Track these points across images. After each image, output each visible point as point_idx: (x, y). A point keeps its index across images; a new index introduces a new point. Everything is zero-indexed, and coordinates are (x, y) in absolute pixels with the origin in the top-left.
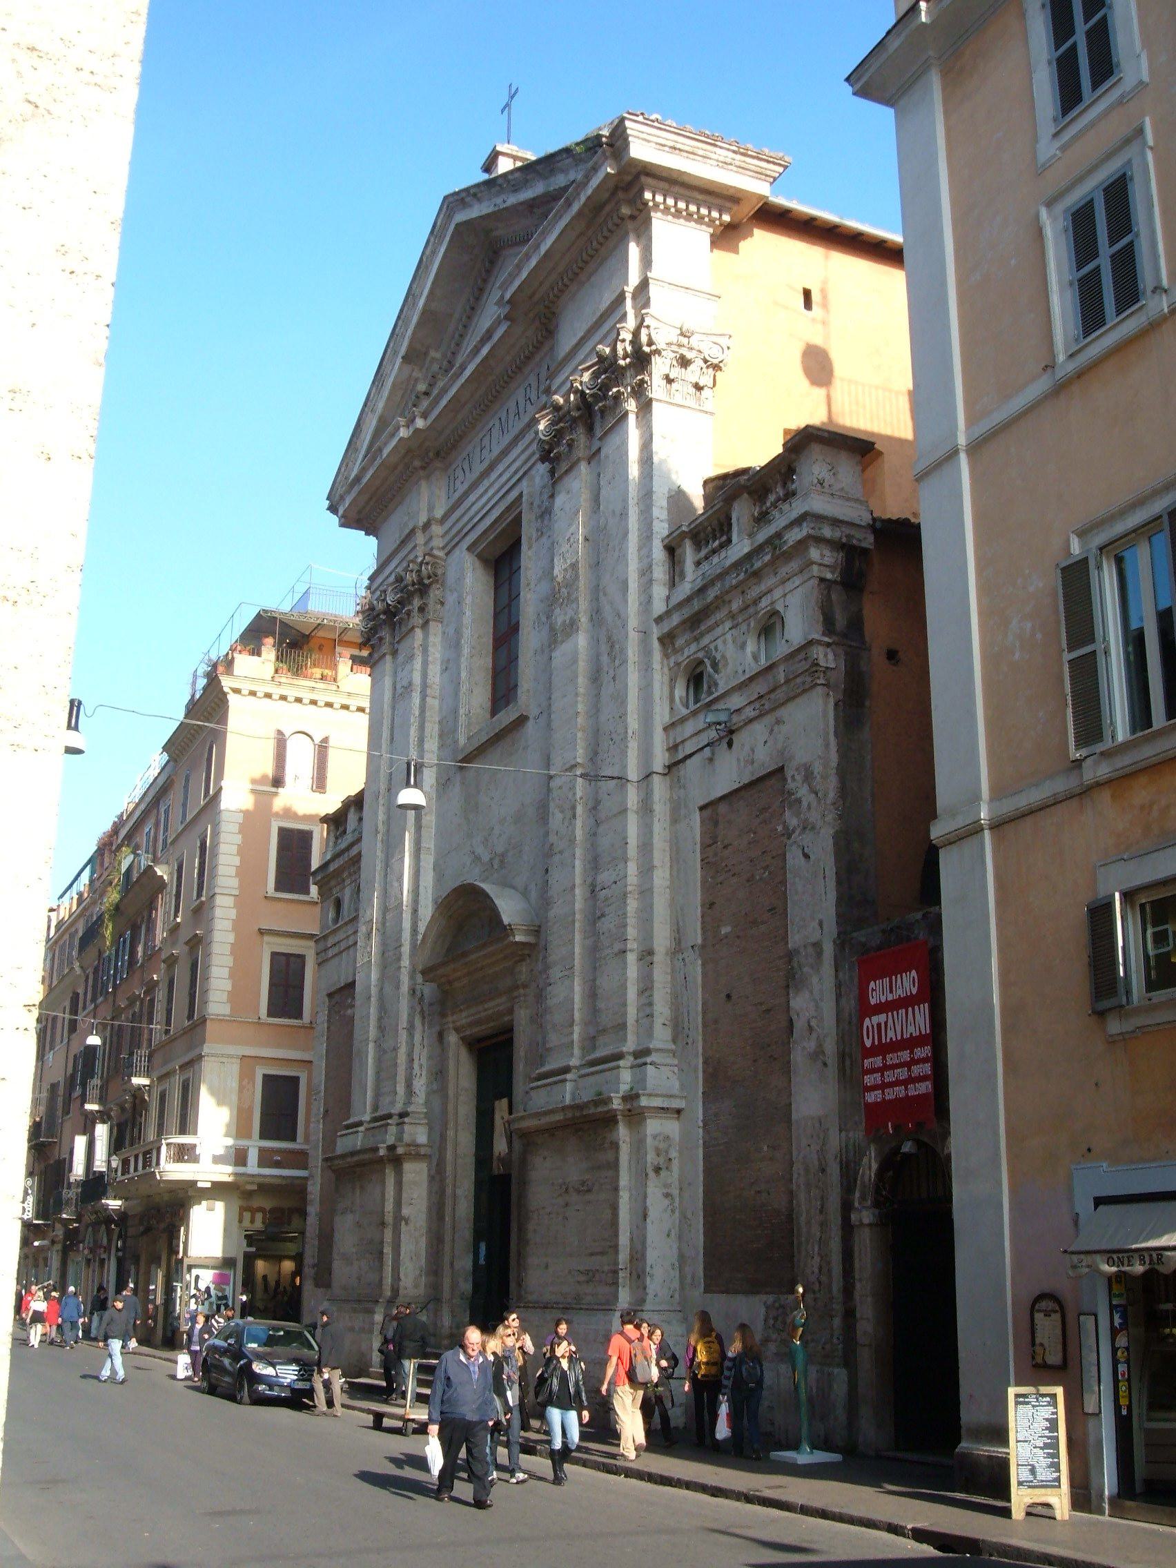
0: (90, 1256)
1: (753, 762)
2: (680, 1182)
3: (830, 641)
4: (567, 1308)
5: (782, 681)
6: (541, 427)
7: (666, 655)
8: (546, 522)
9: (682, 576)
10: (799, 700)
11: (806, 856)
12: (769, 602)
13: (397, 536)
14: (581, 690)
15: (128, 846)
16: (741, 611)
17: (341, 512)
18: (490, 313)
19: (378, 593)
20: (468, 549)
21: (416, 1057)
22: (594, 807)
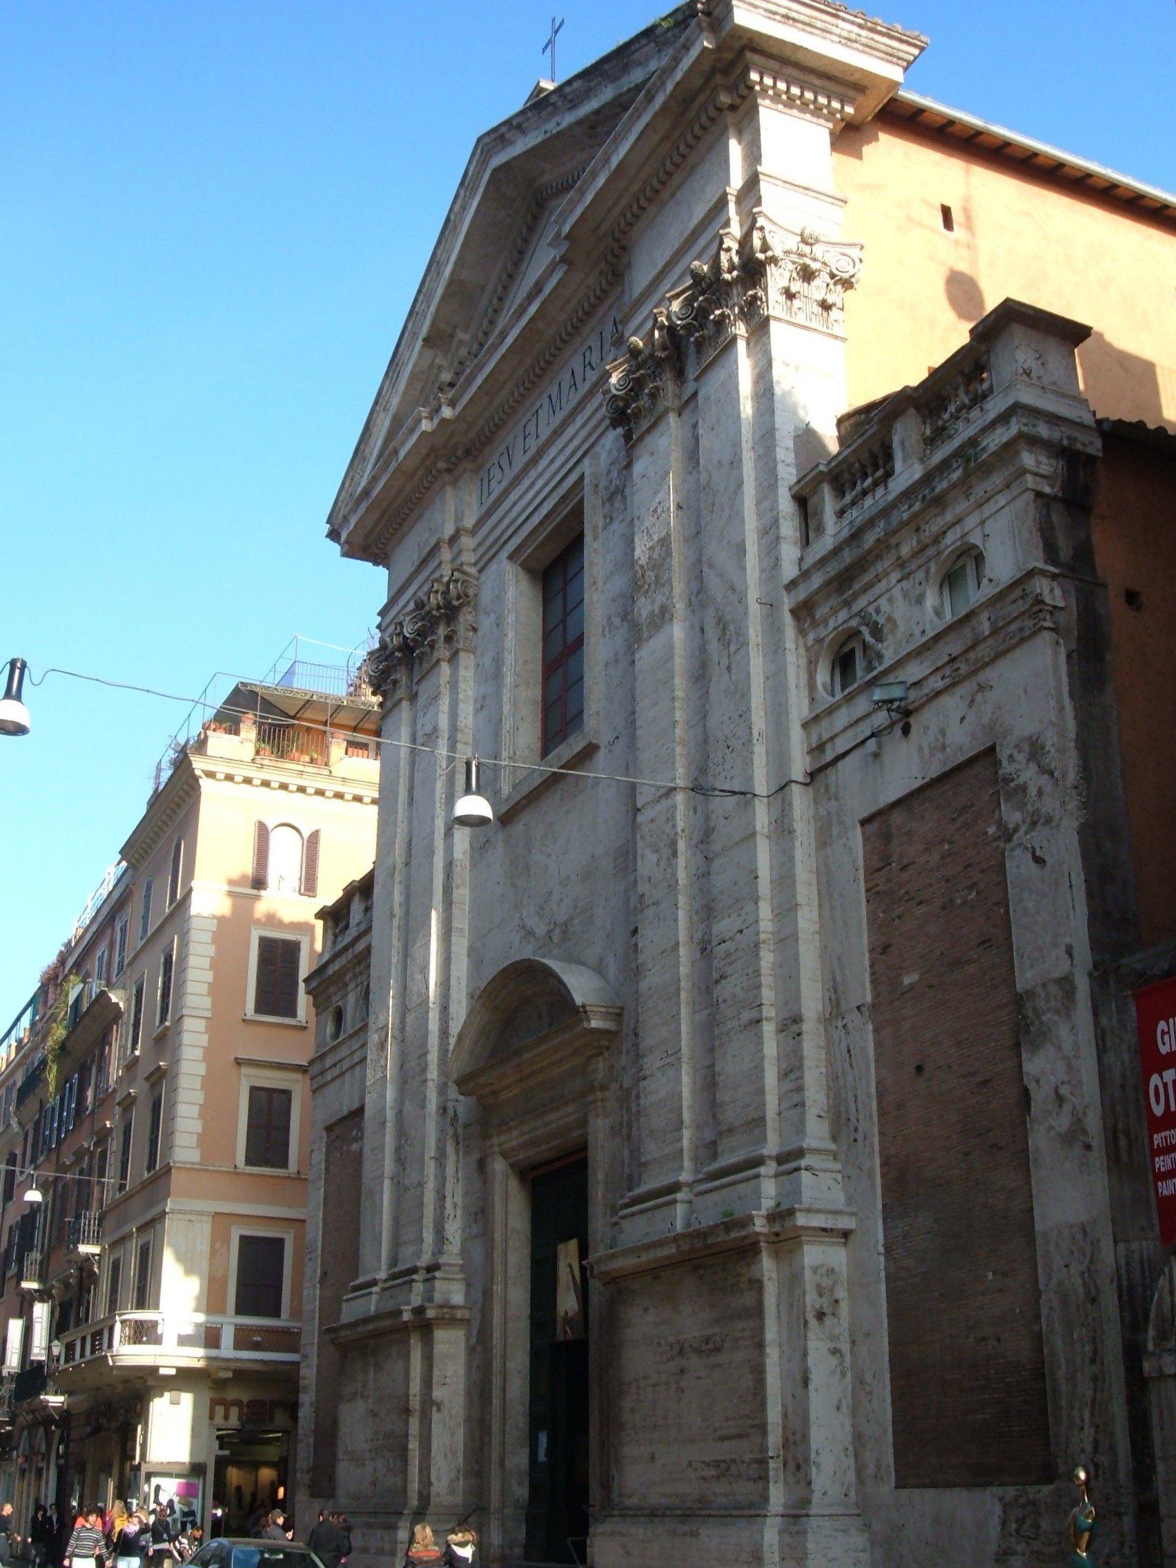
0: (26, 1466)
1: (944, 748)
2: (852, 1332)
3: (1057, 571)
4: (688, 1516)
5: (987, 633)
6: (614, 380)
7: (801, 632)
8: (617, 505)
9: (820, 529)
10: (1017, 653)
11: (1039, 861)
12: (958, 536)
13: (416, 557)
14: (679, 693)
15: (77, 974)
16: (915, 555)
17: (344, 536)
18: (543, 256)
19: (392, 628)
20: (511, 557)
21: (448, 1193)
22: (704, 838)
